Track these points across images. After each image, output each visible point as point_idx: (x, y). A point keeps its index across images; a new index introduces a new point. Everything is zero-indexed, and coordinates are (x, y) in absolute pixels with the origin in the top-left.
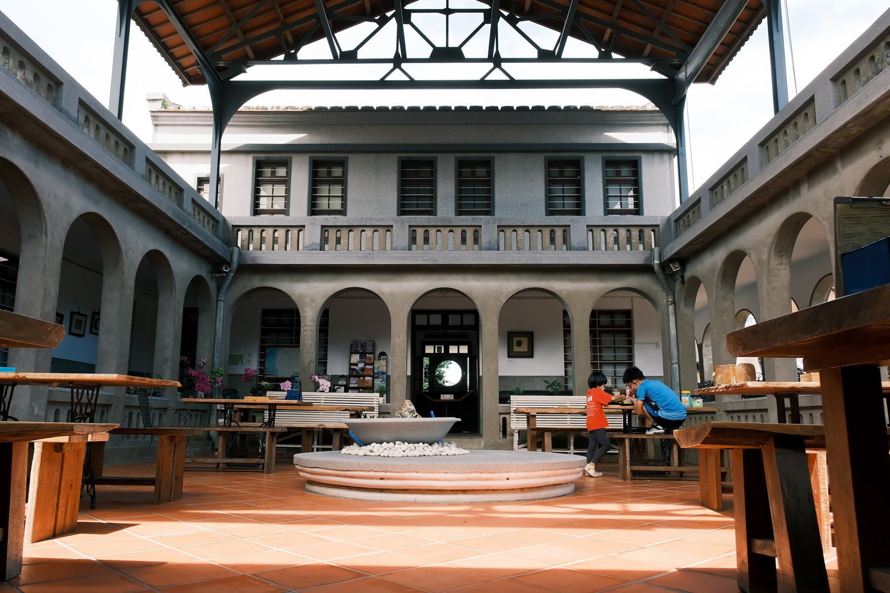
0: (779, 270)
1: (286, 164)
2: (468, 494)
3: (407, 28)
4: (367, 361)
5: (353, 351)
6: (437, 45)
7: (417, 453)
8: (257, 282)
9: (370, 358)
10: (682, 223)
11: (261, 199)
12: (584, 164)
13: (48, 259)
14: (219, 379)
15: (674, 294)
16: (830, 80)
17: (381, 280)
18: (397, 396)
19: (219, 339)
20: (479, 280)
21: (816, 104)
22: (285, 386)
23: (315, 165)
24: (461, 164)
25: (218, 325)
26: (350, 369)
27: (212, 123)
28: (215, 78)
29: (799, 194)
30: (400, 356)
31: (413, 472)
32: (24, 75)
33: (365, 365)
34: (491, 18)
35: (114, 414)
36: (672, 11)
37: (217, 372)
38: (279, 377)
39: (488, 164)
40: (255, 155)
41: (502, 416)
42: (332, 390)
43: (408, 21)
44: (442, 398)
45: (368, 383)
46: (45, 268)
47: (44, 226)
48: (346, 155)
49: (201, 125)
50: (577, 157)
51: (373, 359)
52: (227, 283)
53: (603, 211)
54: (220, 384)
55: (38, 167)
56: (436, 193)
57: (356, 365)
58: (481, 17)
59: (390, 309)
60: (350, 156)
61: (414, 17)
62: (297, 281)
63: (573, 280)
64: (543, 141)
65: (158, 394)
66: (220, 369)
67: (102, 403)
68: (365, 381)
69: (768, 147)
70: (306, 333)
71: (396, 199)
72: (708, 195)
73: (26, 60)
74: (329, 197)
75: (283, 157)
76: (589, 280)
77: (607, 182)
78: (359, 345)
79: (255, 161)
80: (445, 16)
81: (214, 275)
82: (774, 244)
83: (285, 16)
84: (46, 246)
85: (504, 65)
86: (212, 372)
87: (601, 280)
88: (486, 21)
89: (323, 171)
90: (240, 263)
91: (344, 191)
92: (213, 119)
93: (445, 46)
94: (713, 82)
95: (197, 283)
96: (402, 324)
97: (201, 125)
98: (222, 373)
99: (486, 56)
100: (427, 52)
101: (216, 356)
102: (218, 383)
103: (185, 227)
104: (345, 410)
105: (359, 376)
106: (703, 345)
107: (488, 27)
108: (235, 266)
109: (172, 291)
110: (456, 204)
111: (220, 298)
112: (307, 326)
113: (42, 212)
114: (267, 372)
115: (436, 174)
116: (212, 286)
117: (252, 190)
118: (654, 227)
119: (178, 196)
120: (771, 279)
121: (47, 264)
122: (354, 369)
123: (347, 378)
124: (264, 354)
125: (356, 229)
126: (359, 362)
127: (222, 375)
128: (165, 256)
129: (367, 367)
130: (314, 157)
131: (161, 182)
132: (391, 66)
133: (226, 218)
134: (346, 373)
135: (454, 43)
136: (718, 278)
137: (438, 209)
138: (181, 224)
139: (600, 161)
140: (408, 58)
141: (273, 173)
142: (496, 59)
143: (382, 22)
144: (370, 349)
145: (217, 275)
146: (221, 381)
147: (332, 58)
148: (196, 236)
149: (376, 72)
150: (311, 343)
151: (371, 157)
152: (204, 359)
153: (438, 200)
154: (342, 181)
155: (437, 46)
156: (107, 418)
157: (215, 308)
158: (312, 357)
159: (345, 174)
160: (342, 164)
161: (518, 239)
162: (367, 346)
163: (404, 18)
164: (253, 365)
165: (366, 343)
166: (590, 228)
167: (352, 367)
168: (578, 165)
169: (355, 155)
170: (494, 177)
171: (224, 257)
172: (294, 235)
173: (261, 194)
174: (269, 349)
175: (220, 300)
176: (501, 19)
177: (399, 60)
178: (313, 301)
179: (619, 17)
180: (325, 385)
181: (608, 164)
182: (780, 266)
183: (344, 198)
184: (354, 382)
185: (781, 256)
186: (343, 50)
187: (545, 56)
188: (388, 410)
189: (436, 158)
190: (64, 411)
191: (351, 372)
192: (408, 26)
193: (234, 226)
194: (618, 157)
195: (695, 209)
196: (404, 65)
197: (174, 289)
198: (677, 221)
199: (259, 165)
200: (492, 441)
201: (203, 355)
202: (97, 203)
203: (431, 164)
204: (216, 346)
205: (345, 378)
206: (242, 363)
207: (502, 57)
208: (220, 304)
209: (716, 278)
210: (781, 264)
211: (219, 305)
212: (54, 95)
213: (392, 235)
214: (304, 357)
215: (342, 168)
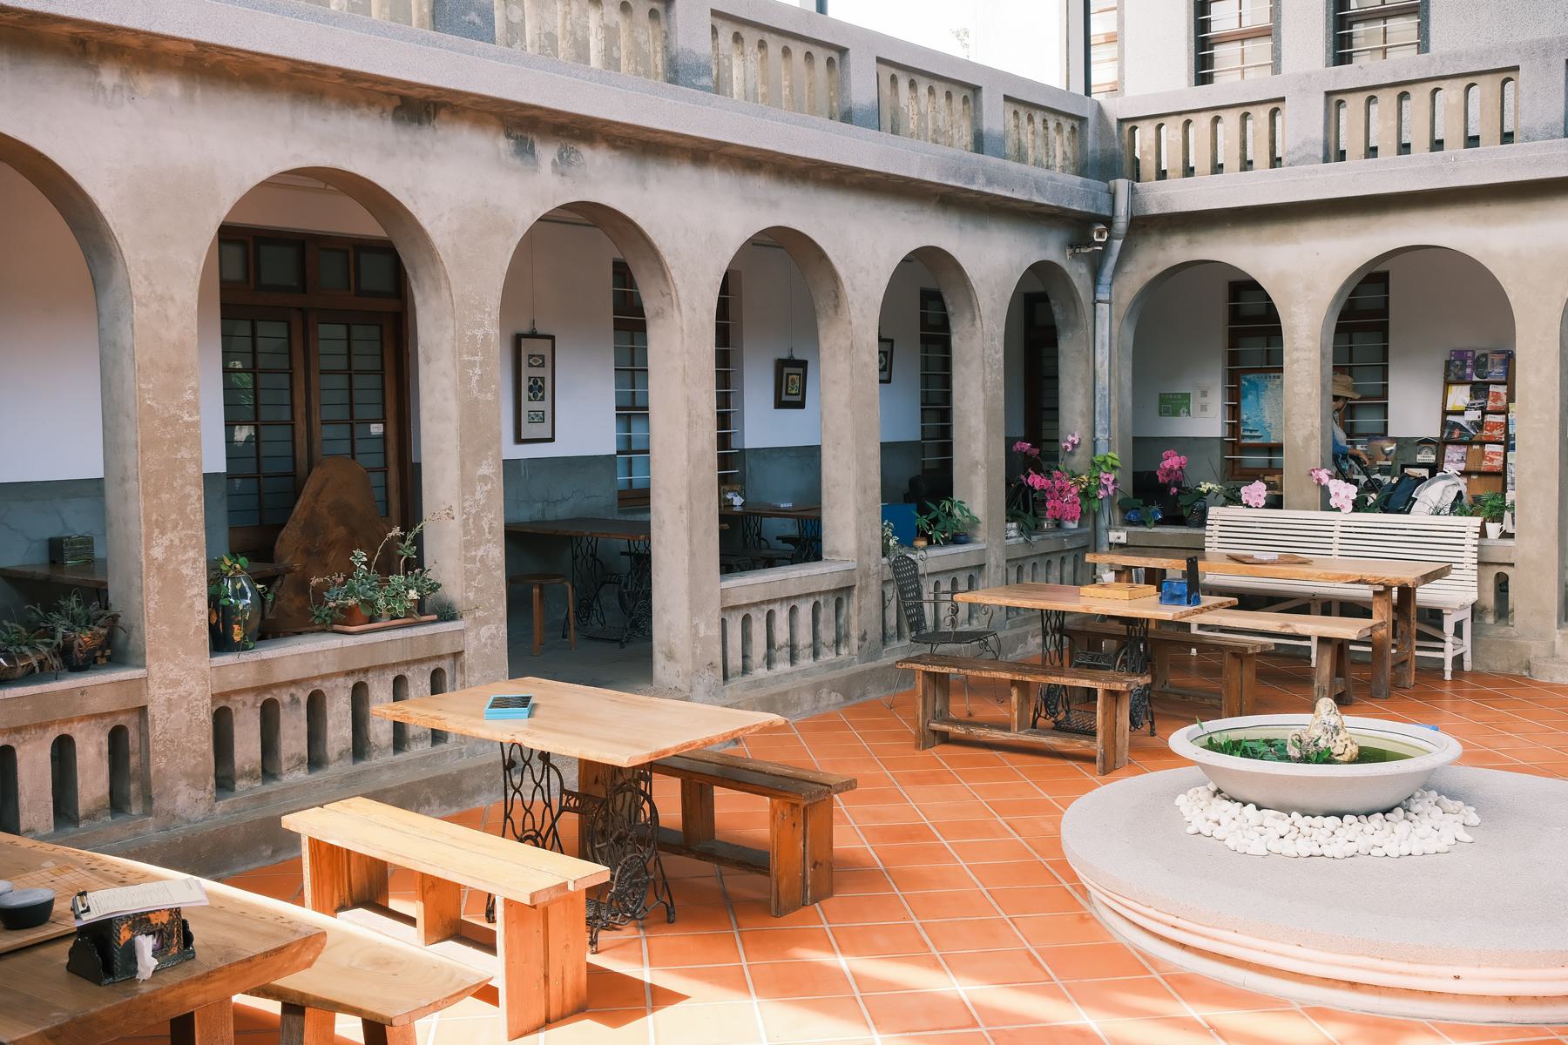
2: (1363, 992)
4: (1490, 405)
5: (1452, 378)
7: (1304, 847)
8: (1179, 250)
9: (1497, 396)
13: (688, 352)
14: (1108, 479)
19: (1104, 388)
22: (1250, 496)
25: (1099, 358)
26: (1445, 424)
31: (1229, 930)
32: (602, 19)
33: (1484, 413)
35: (859, 602)
37: (1105, 462)
38: (1273, 442)
42: (1358, 506)
45: (1492, 460)
47: (673, 294)
51: (1504, 398)
52: (1112, 261)
54: (1111, 488)
57: (1461, 413)
59: (1511, 298)
65: (963, 538)
66: (1109, 454)
67: (832, 587)
68: (1483, 456)
78: (1469, 362)
81: (1077, 251)
84: (682, 330)
86: (1093, 464)
90: (1135, 215)
98: (1116, 463)
101: (1098, 428)
102: (1106, 487)
103: (974, 187)
104: (1359, 582)
105: (1469, 443)
108: (1121, 223)
109: (974, 319)
111: (1100, 297)
112: (1297, 349)
113: (666, 271)
114: (1244, 430)
116: (1078, 273)
119: (971, 104)
121: (687, 364)
122: (1457, 425)
123: (1440, 445)
124: (1237, 389)
125: (1418, 87)
126: (1468, 408)
127: (1114, 467)
128: (945, 251)
129: (1489, 418)
131: (923, 89)
133: (1101, 103)
134: (1434, 432)
138: (963, 186)
144: (1496, 372)
145: (1083, 251)
146: (1115, 482)
148: (1009, 194)
150: (1309, 390)
152: (1073, 435)
156: (848, 610)
157: (1090, 321)
162: (1489, 364)
164: (1207, 421)
165: (1485, 355)
167: (1450, 418)
171: (1092, 211)
172: (1260, 125)
174: (1248, 377)
175: (1099, 301)
180: (1342, 495)
184: (1457, 456)
188: (1509, 557)
191: (1447, 431)
193: (1121, 121)
201: (1073, 426)
202: (774, 204)
204: (1098, 405)
205: (1433, 446)
206: (1189, 413)
208: (1102, 309)
211: (1098, 313)
212: (664, 27)
214: (1294, 424)
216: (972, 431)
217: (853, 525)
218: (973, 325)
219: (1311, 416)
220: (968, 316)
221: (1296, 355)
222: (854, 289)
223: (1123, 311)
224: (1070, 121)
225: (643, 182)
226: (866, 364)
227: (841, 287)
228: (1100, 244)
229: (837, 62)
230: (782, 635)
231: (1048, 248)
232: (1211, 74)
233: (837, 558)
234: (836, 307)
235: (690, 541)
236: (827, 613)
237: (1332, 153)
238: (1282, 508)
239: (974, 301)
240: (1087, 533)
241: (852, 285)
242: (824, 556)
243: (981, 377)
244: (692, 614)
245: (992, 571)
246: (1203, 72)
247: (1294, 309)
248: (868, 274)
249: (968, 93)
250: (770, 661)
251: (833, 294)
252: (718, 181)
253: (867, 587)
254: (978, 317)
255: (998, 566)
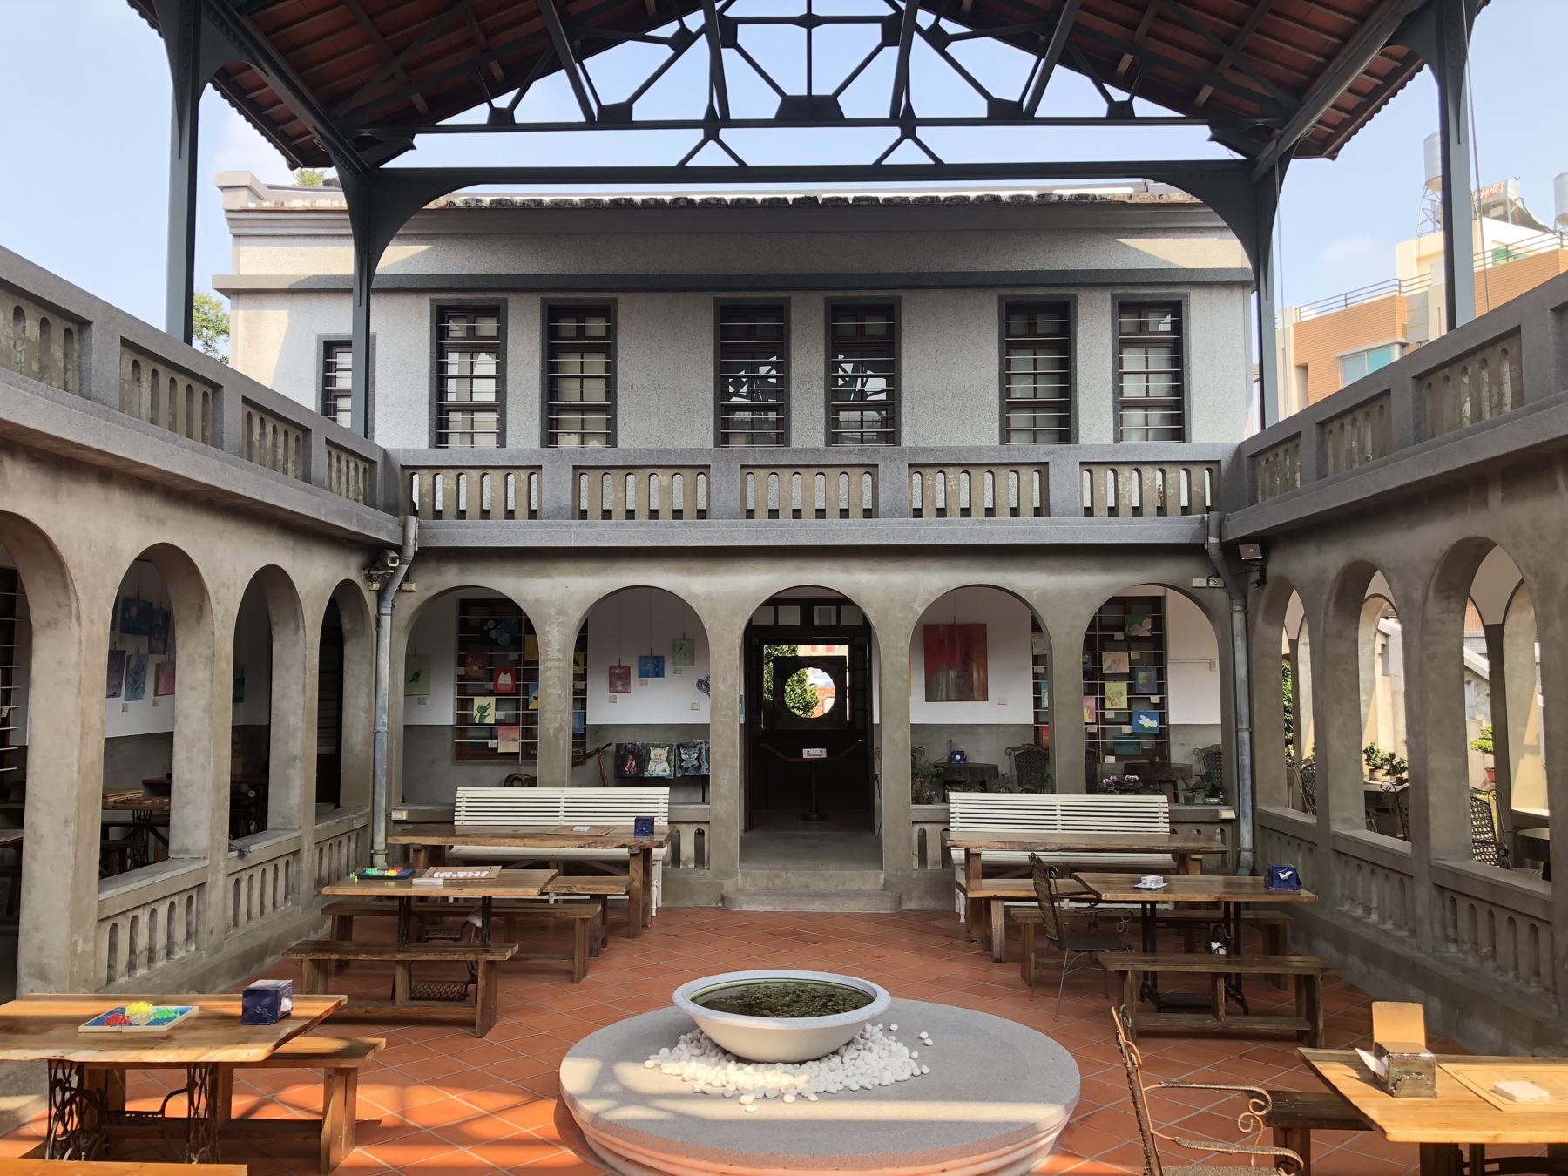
0: (1443, 623)
1: (496, 311)
3: (728, 55)
6: (790, 91)
8: (451, 577)
10: (1263, 463)
11: (450, 381)
12: (1076, 313)
13: (85, 664)
15: (1245, 597)
16: (1552, 310)
17: (690, 572)
18: (722, 790)
20: (874, 571)
21: (1523, 340)
23: (552, 315)
24: (836, 311)
27: (350, 231)
28: (355, 169)
29: (1485, 504)
30: (727, 716)
34: (896, 31)
36: (1258, 31)
39: (890, 312)
40: (435, 296)
41: (917, 828)
43: (732, 42)
44: (805, 756)
46: (80, 683)
47: (74, 605)
48: (613, 295)
49: (327, 236)
50: (1063, 295)
53: (1111, 404)
55: (57, 502)
56: (789, 372)
58: (875, 32)
59: (706, 627)
60: (621, 297)
61: (744, 34)
62: (531, 574)
63: (1052, 570)
64: (995, 267)
69: (1430, 385)
70: (548, 673)
71: (711, 385)
72: (1314, 432)
73: (26, 302)
74: (582, 378)
75: (491, 299)
76: (1084, 570)
77: (1123, 344)
79: (435, 307)
80: (804, 30)
82: (1435, 578)
83: (487, 35)
84: (80, 642)
85: (921, 132)
87: (1107, 569)
88: (888, 40)
89: (568, 325)
91: (611, 367)
92: (349, 224)
93: (804, 93)
94: (1333, 157)
95: (343, 600)
96: (729, 654)
97: (327, 236)
99: (886, 115)
100: (770, 106)
101: (379, 722)
106: (1300, 643)
107: (892, 53)
108: (410, 552)
109: (297, 628)
110: (826, 393)
111: (384, 611)
112: (550, 660)
115: (789, 332)
117: (431, 367)
118: (1211, 465)
120: (1427, 638)
121: (83, 675)
125: (640, 471)
130: (552, 299)
132: (699, 134)
135: (822, 88)
136: (1329, 599)
137: (792, 404)
139: (1109, 303)
140: (731, 118)
141: (472, 331)
142: (904, 120)
143: (682, 42)
147: (582, 119)
149: (666, 149)
151: (660, 300)
153: (793, 384)
154: (606, 347)
155: (789, 93)
158: (562, 719)
159: (611, 332)
160: (606, 312)
161: (948, 489)
163: (723, 33)
166: (1087, 465)
168: (1064, 312)
169: (630, 296)
170: (900, 338)
172: (521, 484)
173: (450, 373)
176: (916, 36)
177: (715, 122)
178: (560, 612)
179: (1150, 33)
181: (1123, 307)
182: (1445, 615)
183: (611, 381)
185: (1448, 598)
186: (604, 102)
187: (1004, 113)
189: (788, 300)
190: (125, 923)
192: (733, 51)
193: (403, 467)
194: (1144, 295)
195: (1290, 446)
196: (724, 134)
197: (301, 624)
198: (1254, 457)
199: (441, 316)
200: (899, 874)
202: (162, 522)
203: (780, 311)
207: (917, 116)
209: (1324, 597)
210: (1448, 611)
213: (708, 484)
215: (605, 319)
216: (291, 728)
217: (207, 824)
218: (296, 634)
219: (560, 712)
220: (292, 626)
221: (549, 664)
222: (218, 603)
223: (403, 623)
224: (364, 463)
225: (56, 495)
226: (223, 672)
227: (207, 601)
228: (392, 568)
229: (210, 397)
230: (142, 942)
231: (347, 568)
232: (447, 434)
233: (188, 856)
234: (199, 619)
235: (75, 855)
236: (181, 911)
237: (578, 513)
238: (536, 786)
239: (300, 613)
240: (367, 814)
241: (217, 599)
242: (171, 855)
243: (302, 680)
244: (72, 932)
245: (305, 855)
246: (440, 438)
247: (548, 628)
248: (228, 590)
249: (300, 434)
250: (131, 967)
251: (197, 607)
252: (119, 499)
253: (216, 881)
254: (301, 628)
255: (309, 850)
